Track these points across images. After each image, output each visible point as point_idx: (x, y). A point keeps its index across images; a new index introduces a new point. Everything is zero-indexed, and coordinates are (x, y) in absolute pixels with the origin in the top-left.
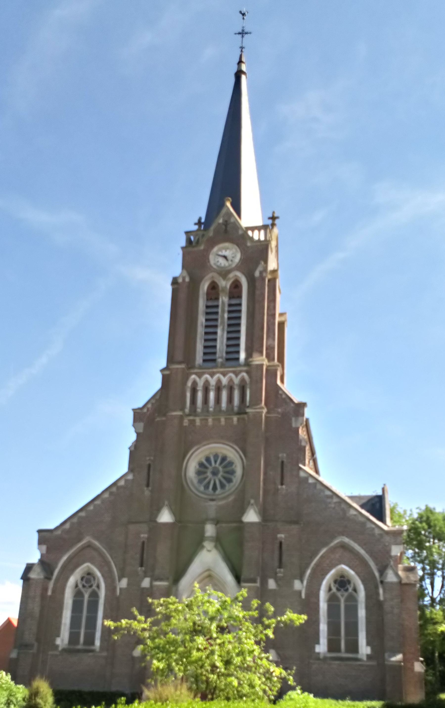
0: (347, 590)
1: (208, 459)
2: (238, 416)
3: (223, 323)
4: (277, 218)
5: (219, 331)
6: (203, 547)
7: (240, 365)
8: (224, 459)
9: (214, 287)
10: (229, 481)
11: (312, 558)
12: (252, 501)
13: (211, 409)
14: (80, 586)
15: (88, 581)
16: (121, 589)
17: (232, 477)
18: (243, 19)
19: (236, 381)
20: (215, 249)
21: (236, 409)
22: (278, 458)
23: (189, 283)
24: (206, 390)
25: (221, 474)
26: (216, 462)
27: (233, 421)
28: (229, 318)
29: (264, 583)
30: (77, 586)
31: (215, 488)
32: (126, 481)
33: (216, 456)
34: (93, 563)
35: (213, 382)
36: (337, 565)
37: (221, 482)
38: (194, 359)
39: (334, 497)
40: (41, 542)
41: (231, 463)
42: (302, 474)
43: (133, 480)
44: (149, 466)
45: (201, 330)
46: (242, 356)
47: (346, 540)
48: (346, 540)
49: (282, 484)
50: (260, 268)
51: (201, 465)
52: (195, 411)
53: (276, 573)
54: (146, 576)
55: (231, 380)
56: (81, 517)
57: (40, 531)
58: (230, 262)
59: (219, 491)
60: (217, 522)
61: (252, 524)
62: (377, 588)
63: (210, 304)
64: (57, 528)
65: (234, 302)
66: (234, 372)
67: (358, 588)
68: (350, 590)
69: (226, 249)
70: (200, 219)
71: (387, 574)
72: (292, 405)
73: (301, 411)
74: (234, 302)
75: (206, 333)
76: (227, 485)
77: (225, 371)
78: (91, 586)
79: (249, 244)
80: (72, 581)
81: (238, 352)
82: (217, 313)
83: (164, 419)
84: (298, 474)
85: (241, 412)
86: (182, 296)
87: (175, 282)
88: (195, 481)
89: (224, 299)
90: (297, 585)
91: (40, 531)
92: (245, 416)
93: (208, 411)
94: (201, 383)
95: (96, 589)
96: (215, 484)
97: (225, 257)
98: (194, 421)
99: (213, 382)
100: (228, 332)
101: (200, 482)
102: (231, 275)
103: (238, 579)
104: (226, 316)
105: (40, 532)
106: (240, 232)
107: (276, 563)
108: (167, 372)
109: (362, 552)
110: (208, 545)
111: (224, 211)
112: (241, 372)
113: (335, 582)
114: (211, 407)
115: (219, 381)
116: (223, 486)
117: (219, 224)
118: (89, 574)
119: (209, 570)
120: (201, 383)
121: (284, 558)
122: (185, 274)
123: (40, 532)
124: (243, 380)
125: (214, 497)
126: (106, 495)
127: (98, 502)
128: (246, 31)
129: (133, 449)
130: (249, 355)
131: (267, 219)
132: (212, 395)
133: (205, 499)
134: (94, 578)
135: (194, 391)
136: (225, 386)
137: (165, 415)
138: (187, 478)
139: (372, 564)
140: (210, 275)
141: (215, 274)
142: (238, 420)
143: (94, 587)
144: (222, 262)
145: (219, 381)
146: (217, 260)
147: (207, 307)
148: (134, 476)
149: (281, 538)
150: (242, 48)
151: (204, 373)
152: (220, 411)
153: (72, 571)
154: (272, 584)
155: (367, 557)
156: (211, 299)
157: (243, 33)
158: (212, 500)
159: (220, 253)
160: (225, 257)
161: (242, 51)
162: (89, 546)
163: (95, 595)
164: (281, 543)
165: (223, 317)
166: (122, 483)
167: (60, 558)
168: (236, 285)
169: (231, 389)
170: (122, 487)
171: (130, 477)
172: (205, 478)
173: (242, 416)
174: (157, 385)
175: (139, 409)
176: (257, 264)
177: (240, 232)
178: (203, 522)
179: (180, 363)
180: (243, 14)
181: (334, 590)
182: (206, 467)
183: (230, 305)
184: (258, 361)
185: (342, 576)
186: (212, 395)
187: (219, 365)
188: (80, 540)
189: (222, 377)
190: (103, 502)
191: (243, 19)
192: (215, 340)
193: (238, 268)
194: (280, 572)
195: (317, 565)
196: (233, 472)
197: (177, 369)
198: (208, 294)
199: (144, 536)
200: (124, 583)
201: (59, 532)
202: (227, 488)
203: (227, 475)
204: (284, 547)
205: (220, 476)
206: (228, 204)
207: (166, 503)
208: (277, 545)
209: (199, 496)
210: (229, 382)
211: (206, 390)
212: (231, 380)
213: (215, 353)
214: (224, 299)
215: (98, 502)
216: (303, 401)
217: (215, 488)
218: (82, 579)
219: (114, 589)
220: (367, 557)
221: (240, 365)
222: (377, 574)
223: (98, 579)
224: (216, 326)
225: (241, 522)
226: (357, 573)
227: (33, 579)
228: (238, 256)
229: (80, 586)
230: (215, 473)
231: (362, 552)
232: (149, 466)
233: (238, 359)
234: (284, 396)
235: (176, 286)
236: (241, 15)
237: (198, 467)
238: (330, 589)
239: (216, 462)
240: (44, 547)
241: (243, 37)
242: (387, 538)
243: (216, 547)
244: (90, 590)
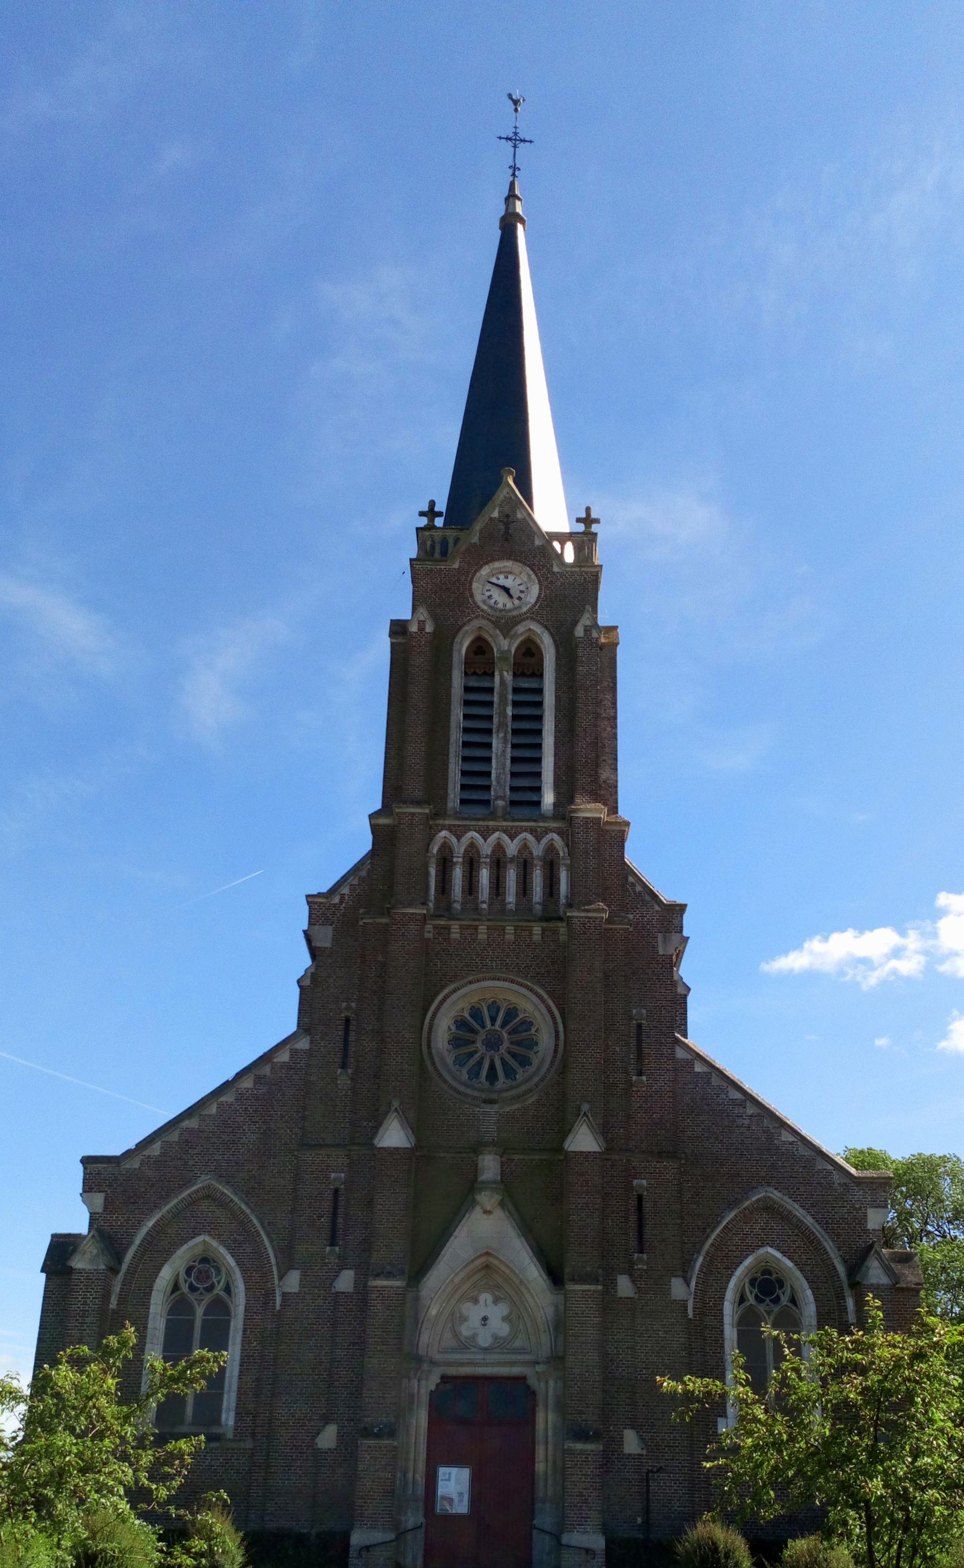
0: (777, 1300)
1: (476, 1013)
2: (545, 924)
3: (502, 725)
4: (597, 521)
5: (496, 742)
6: (474, 1203)
7: (544, 818)
8: (512, 1013)
9: (480, 648)
10: (524, 1062)
11: (705, 1231)
12: (585, 1107)
13: (457, 906)
14: (185, 1288)
15: (203, 1276)
16: (284, 1295)
17: (531, 1054)
18: (516, 110)
19: (538, 850)
20: (485, 571)
21: (512, 906)
22: (631, 1018)
23: (435, 634)
24: (472, 865)
25: (506, 1044)
26: (493, 1020)
27: (531, 934)
28: (515, 717)
29: (610, 1285)
30: (176, 1287)
31: (492, 1076)
32: (294, 1052)
33: (494, 1008)
34: (218, 1237)
35: (486, 848)
36: (759, 1247)
37: (504, 1063)
38: (445, 797)
39: (748, 1104)
40: (89, 1187)
41: (527, 1024)
42: (680, 1054)
43: (309, 1053)
44: (347, 1021)
45: (456, 737)
46: (548, 798)
47: (776, 1195)
48: (776, 1195)
49: (640, 1074)
50: (585, 620)
51: (461, 1023)
52: (449, 908)
53: (631, 1263)
54: (342, 1267)
55: (525, 847)
56: (190, 1131)
57: (86, 1161)
58: (517, 602)
59: (502, 1081)
60: (504, 1149)
61: (586, 1155)
62: (841, 1297)
63: (474, 683)
64: (128, 1154)
65: (525, 684)
66: (532, 831)
67: (800, 1296)
68: (784, 1300)
69: (507, 574)
70: (432, 504)
71: (868, 1268)
72: (657, 908)
73: (676, 922)
74: (525, 684)
75: (466, 744)
76: (520, 1071)
77: (512, 827)
78: (210, 1289)
79: (556, 569)
80: (166, 1275)
81: (538, 789)
82: (490, 704)
83: (385, 920)
84: (673, 1053)
85: (550, 915)
86: (419, 662)
87: (398, 629)
88: (450, 1060)
89: (503, 677)
90: (678, 1289)
91: (86, 1161)
92: (562, 928)
93: (476, 909)
94: (459, 848)
95: (222, 1293)
96: (492, 1067)
97: (506, 590)
98: (448, 928)
99: (486, 848)
100: (514, 746)
101: (459, 1061)
102: (520, 629)
103: (555, 1276)
104: (509, 711)
105: (87, 1161)
106: (538, 542)
107: (633, 1243)
108: (383, 821)
109: (809, 1220)
110: (487, 1199)
111: (501, 494)
112: (547, 831)
113: (752, 1282)
114: (483, 902)
115: (499, 848)
116: (510, 1073)
117: (491, 519)
118: (205, 1260)
119: (487, 1254)
120: (459, 848)
121: (648, 1231)
122: (423, 614)
123: (87, 1161)
124: (551, 848)
125: (494, 1096)
126: (247, 1083)
127: (228, 1098)
128: (521, 135)
129: (307, 982)
130: (565, 795)
131: (575, 520)
132: (484, 875)
133: (475, 1098)
134: (218, 1270)
135: (445, 864)
136: (512, 860)
137: (388, 912)
138: (434, 1051)
139: (829, 1246)
140: (476, 623)
141: (484, 623)
142: (544, 930)
143: (219, 1290)
144: (500, 599)
145: (499, 847)
146: (488, 594)
147: (467, 689)
148: (312, 1042)
149: (641, 1186)
150: (514, 168)
151: (467, 829)
152: (503, 910)
153: (167, 1254)
154: (624, 1287)
155: (817, 1229)
156: (475, 673)
157: (515, 140)
158: (491, 1102)
159: (494, 580)
160: (506, 590)
161: (514, 175)
162: (209, 1195)
163: (220, 1308)
164: (640, 1198)
165: (503, 714)
166: (284, 1057)
167: (140, 1222)
168: (530, 650)
169: (525, 866)
170: (283, 1065)
171: (303, 1044)
172: (471, 1055)
173: (552, 924)
174: (364, 843)
175: (320, 895)
176: (581, 612)
177: (538, 542)
178: (477, 1148)
179: (418, 803)
180: (516, 102)
181: (751, 1300)
182: (473, 1031)
183: (516, 690)
184: (590, 810)
185: (766, 1272)
186: (484, 875)
187: (500, 813)
188: (187, 1183)
189: (505, 838)
190: (240, 1098)
191: (516, 110)
192: (489, 760)
193: (533, 615)
194: (641, 1260)
195: (716, 1246)
196: (531, 1044)
197: (413, 814)
198: (468, 662)
199: (338, 1177)
200: (293, 1281)
201: (135, 1164)
202: (519, 1077)
203: (516, 1049)
204: (647, 1206)
205: (503, 1049)
206: (511, 481)
207: (396, 1104)
208: (633, 1203)
209: (459, 1093)
210: (493, 852)
211: (472, 865)
212: (525, 847)
213: (488, 788)
214: (503, 677)
215: (228, 1098)
216: (686, 903)
217: (492, 1076)
218: (189, 1271)
219: (268, 1296)
220: (817, 1229)
221: (544, 818)
222: (841, 1269)
223: (229, 1274)
224: (489, 732)
225: (373, 1146)
226: (799, 1265)
227: (80, 1271)
228: (535, 590)
229: (185, 1288)
230: (493, 1043)
231: (809, 1220)
232: (347, 1021)
233: (538, 804)
234: (638, 888)
235: (400, 640)
236: (511, 102)
237: (453, 1028)
238: (742, 1299)
239: (493, 1020)
240: (99, 1199)
241: (515, 147)
242: (859, 1194)
243: (502, 1204)
244: (208, 1298)
